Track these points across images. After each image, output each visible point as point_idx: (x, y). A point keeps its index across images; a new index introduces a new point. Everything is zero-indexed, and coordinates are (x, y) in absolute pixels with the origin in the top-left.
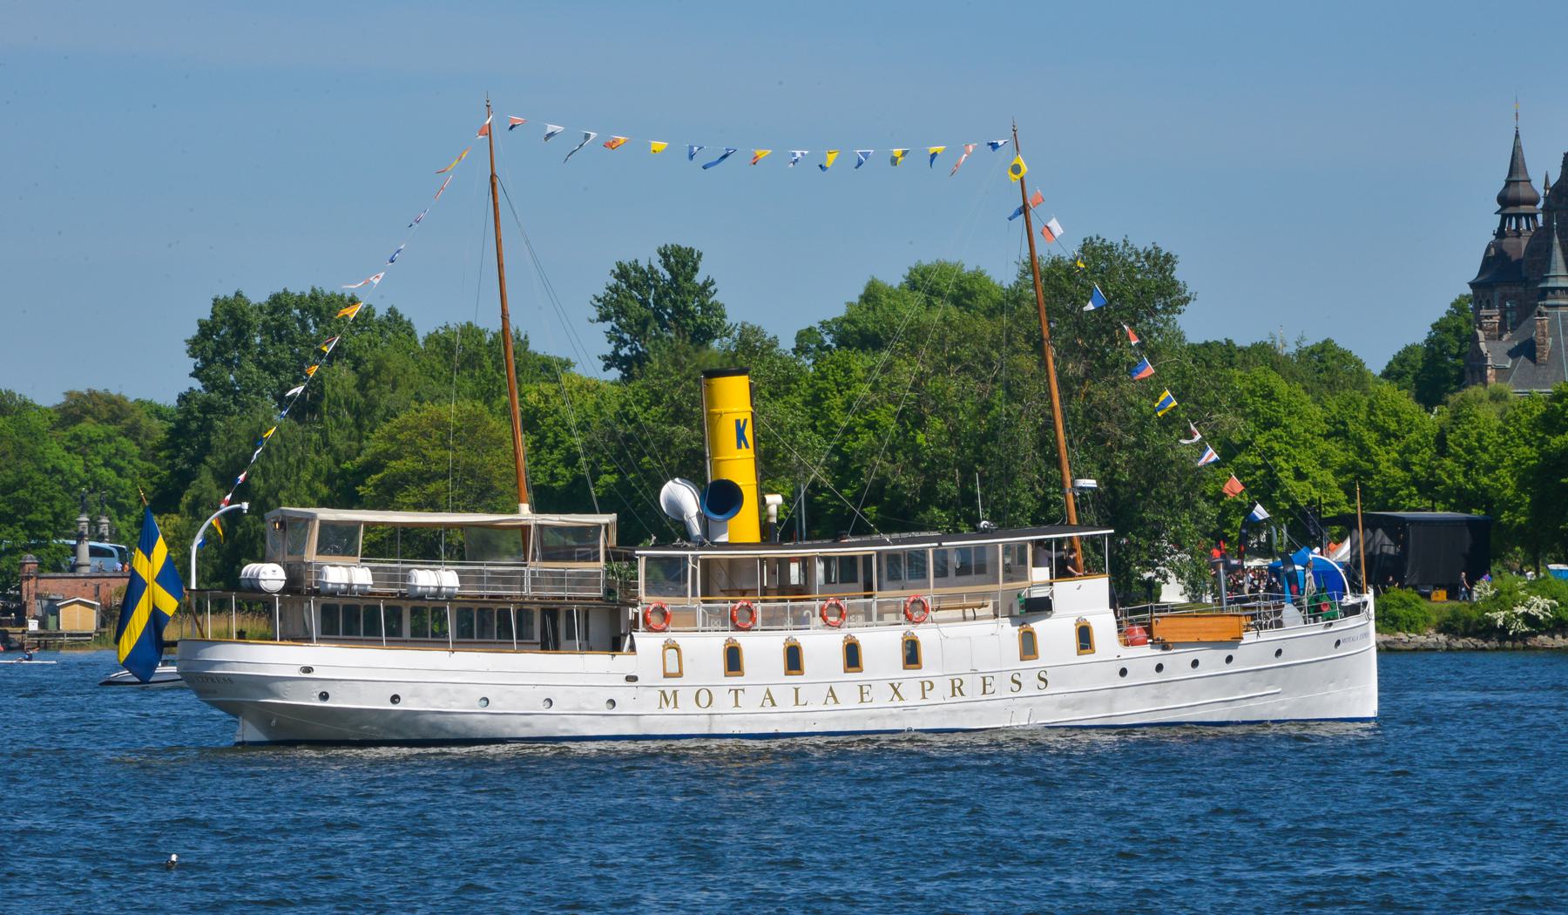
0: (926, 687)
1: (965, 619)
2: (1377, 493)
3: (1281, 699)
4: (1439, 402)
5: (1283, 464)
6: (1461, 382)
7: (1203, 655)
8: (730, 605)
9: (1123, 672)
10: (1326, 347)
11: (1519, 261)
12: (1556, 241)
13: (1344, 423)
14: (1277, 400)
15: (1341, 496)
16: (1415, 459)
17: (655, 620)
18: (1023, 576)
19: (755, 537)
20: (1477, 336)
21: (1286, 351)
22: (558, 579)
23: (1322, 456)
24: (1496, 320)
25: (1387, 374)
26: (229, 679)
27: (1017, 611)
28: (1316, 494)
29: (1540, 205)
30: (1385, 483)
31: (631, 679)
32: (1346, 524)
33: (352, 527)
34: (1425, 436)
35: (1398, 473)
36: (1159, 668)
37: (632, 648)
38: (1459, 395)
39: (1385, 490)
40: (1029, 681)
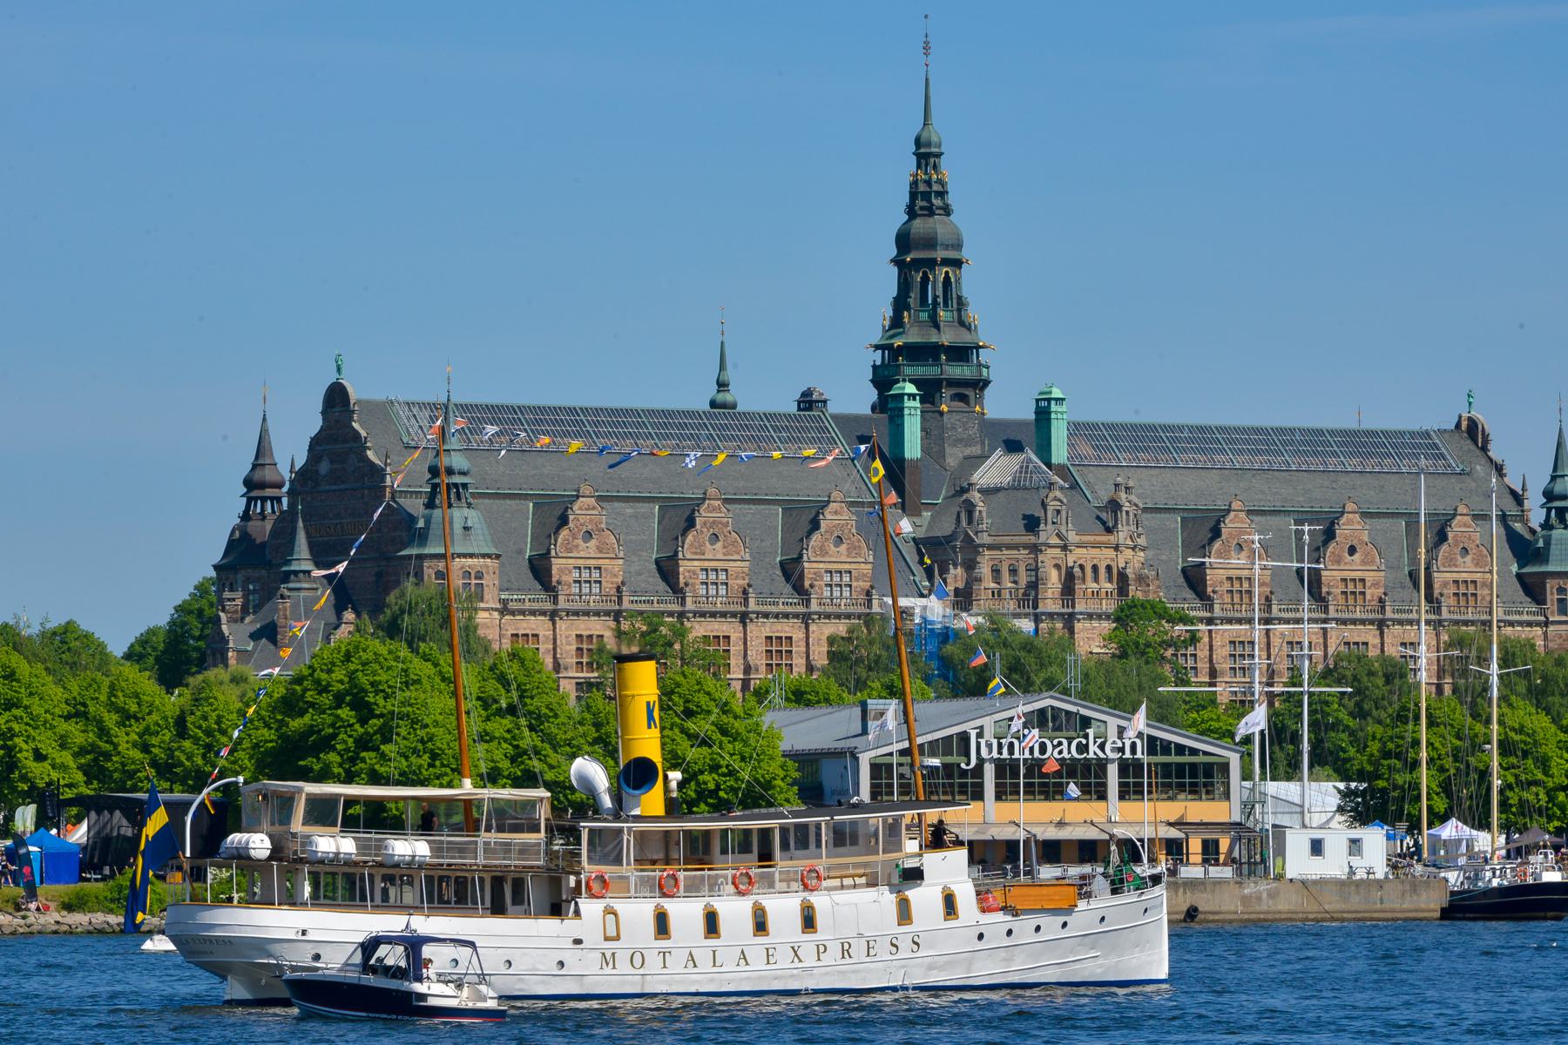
0: (821, 949)
1: (843, 887)
2: (116, 775)
3: (1100, 961)
4: (180, 684)
5: (25, 746)
6: (202, 665)
7: (1043, 920)
8: (658, 874)
9: (981, 937)
10: (68, 629)
11: (263, 544)
12: (301, 524)
13: (84, 705)
14: (18, 681)
15: (80, 777)
16: (154, 741)
17: (596, 887)
18: (898, 847)
19: (661, 811)
20: (219, 619)
21: (30, 631)
22: (506, 848)
23: (62, 737)
24: (239, 602)
25: (128, 656)
26: (228, 941)
27: (896, 880)
28: (55, 775)
29: (285, 489)
30: (123, 764)
31: (578, 942)
32: (85, 805)
33: (332, 800)
34: (165, 718)
35: (137, 754)
36: (1010, 932)
37: (577, 913)
38: (200, 677)
39: (124, 771)
40: (905, 944)
